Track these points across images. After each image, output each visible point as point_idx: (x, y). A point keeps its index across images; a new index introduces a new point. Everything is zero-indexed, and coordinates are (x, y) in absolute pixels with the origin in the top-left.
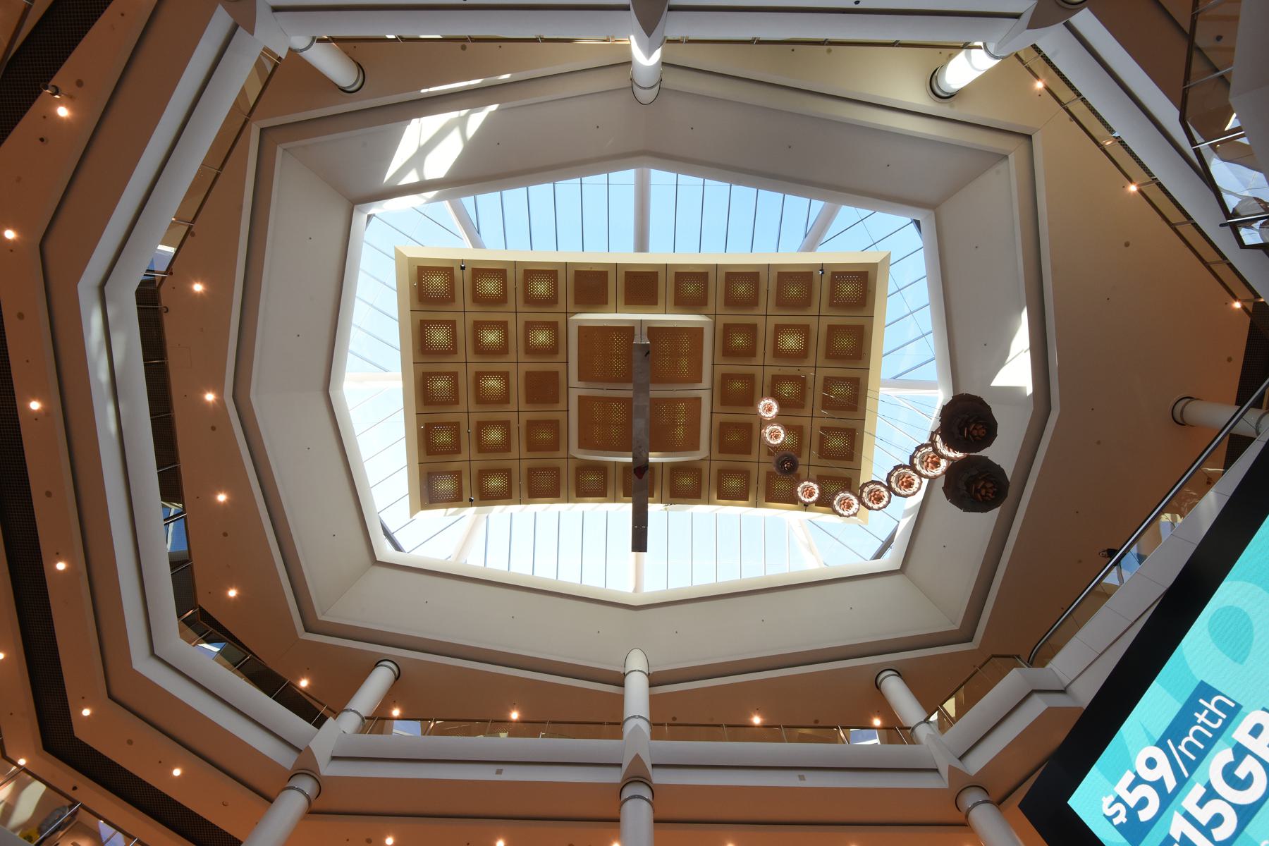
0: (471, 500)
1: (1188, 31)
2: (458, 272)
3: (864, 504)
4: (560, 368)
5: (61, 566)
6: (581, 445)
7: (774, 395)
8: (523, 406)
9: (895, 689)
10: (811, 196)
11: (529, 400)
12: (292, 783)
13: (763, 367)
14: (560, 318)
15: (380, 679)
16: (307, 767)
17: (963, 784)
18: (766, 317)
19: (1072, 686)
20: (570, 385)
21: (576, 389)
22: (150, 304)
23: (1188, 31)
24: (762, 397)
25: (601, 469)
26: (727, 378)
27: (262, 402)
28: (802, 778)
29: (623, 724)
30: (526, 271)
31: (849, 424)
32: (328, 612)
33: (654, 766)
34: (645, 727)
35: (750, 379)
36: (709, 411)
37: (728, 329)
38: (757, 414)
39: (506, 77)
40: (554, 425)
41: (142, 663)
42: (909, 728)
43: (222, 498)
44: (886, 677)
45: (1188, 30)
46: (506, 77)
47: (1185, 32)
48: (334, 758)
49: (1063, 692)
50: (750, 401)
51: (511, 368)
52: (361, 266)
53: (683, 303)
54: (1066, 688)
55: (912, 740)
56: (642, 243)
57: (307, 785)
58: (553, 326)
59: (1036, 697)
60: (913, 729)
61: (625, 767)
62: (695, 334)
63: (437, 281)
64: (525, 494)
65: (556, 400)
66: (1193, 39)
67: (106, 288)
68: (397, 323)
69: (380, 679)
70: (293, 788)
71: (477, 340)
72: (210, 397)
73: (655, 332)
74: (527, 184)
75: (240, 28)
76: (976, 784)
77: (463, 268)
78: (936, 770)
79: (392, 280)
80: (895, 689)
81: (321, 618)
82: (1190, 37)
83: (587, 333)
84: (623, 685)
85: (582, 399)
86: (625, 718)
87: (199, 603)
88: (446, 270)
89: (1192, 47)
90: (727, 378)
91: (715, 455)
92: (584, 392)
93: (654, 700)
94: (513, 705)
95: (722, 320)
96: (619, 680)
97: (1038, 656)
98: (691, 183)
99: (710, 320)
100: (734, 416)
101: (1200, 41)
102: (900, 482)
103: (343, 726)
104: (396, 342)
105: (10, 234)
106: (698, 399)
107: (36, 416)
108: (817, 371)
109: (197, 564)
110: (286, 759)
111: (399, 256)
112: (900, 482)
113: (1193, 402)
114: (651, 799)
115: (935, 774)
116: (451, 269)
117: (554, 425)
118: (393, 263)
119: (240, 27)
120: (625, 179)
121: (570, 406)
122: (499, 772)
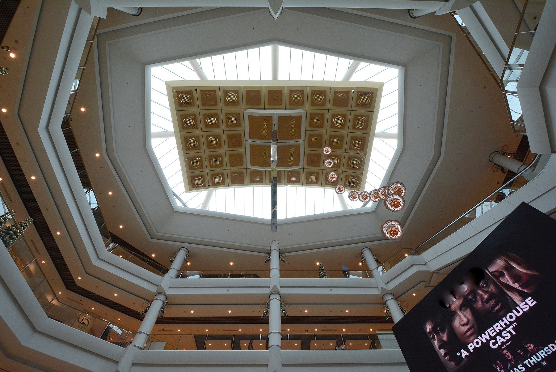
1: (521, 12)
3: (360, 199)
4: (242, 132)
6: (252, 164)
7: (330, 145)
9: (368, 255)
10: (350, 59)
11: (229, 147)
12: (155, 298)
13: (326, 132)
14: (241, 111)
16: (161, 292)
17: (386, 293)
18: (328, 110)
19: (428, 263)
20: (246, 140)
22: (67, 127)
23: (521, 12)
24: (326, 146)
25: (260, 173)
26: (311, 136)
28: (331, 290)
29: (270, 271)
33: (281, 287)
35: (320, 136)
36: (304, 130)
37: (312, 116)
40: (312, 125)
41: (96, 262)
42: (370, 271)
43: (110, 193)
44: (364, 251)
45: (521, 11)
47: (520, 12)
49: (425, 264)
50: (320, 146)
52: (152, 86)
53: (294, 104)
55: (372, 277)
58: (238, 115)
61: (271, 288)
62: (299, 118)
63: (185, 97)
64: (230, 182)
65: (240, 146)
66: (523, 15)
67: (49, 128)
71: (206, 122)
72: (97, 155)
73: (281, 119)
75: (82, 10)
76: (391, 293)
77: (196, 90)
78: (377, 287)
79: (165, 92)
80: (368, 255)
82: (522, 15)
83: (251, 118)
85: (251, 146)
87: (109, 230)
89: (522, 18)
90: (311, 136)
91: (306, 167)
92: (252, 143)
95: (309, 112)
96: (269, 252)
97: (418, 251)
98: (297, 52)
99: (305, 111)
100: (314, 151)
101: (525, 16)
102: (374, 196)
103: (172, 273)
105: (4, 110)
108: (349, 133)
109: (103, 213)
110: (154, 289)
112: (374, 196)
113: (499, 154)
115: (377, 289)
116: (192, 91)
119: (82, 9)
120: (267, 50)
122: (228, 291)
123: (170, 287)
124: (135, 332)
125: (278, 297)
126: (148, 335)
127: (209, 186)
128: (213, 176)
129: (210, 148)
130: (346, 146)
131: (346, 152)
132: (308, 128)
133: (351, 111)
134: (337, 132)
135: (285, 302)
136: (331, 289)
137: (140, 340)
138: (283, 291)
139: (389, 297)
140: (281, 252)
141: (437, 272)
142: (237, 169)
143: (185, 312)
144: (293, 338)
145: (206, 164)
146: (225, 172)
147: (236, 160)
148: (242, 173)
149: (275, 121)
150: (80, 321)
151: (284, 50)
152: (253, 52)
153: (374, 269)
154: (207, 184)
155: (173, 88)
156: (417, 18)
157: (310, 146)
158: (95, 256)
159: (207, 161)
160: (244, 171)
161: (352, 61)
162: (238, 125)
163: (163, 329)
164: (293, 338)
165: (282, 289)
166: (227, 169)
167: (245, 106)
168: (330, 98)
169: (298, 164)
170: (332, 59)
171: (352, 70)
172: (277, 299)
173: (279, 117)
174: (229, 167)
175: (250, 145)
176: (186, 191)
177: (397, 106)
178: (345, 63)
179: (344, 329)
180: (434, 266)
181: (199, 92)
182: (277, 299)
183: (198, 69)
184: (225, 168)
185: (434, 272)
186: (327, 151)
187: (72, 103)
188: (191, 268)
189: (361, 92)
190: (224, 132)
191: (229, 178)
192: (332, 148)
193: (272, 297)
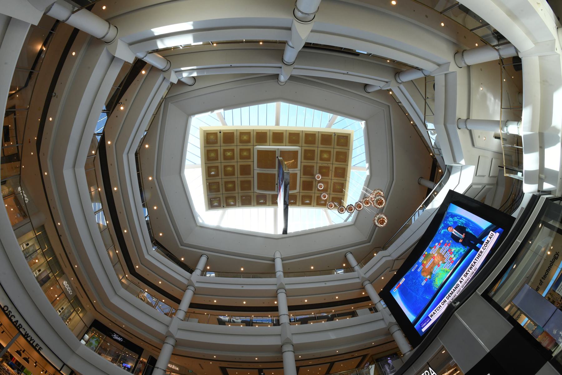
0: (223, 206)
2: (219, 134)
4: (251, 163)
5: (125, 231)
6: (258, 188)
8: (239, 176)
9: (351, 258)
12: (187, 288)
13: (317, 164)
14: (251, 147)
15: (203, 260)
16: (191, 284)
17: (364, 280)
18: (318, 148)
21: (256, 170)
25: (264, 197)
27: (164, 180)
28: (325, 284)
30: (240, 133)
31: (342, 182)
32: (186, 241)
34: (282, 274)
38: (315, 178)
39: (292, 201)
40: (249, 182)
41: (147, 257)
46: (292, 201)
48: (197, 282)
51: (235, 164)
54: (390, 255)
56: (277, 123)
57: (192, 288)
58: (249, 150)
59: (384, 258)
60: (354, 267)
62: (296, 153)
63: (212, 137)
68: (200, 149)
69: (203, 260)
70: (189, 289)
72: (150, 178)
74: (241, 107)
80: (351, 258)
81: (185, 242)
83: (260, 152)
84: (274, 261)
86: (276, 271)
88: (215, 134)
92: (259, 172)
93: (283, 265)
94: (242, 267)
95: (304, 148)
96: (273, 260)
97: (384, 248)
98: (294, 108)
103: (197, 272)
104: (199, 155)
106: (296, 174)
107: (116, 192)
108: (334, 165)
111: (201, 129)
114: (285, 292)
115: (358, 279)
117: (249, 182)
118: (199, 130)
120: (272, 106)
121: (254, 175)
122: (242, 287)
123: (197, 282)
124: (177, 310)
125: (284, 291)
126: (185, 312)
127: (223, 206)
128: (227, 198)
129: (234, 173)
130: (332, 173)
131: (332, 179)
132: (303, 161)
133: (335, 149)
134: (324, 164)
135: (289, 294)
136: (325, 283)
137: (181, 314)
138: (287, 287)
139: (367, 282)
140: (283, 260)
141: (397, 259)
142: (246, 192)
143: (210, 301)
144: (296, 321)
145: (222, 188)
146: (236, 195)
147: (246, 186)
148: (250, 196)
149: (278, 154)
150: (140, 296)
151: (284, 105)
152: (262, 107)
153: (377, 303)
154: (222, 205)
155: (204, 131)
156: (369, 93)
157: (304, 174)
158: (147, 253)
159: (223, 186)
160: (252, 194)
161: (331, 115)
162: (248, 157)
163: (194, 312)
164: (296, 321)
165: (286, 285)
166: (238, 192)
167: (255, 144)
168: (319, 139)
169: (295, 189)
170: (318, 113)
171: (331, 123)
172: (283, 292)
173: (281, 151)
174: (240, 191)
175: (258, 173)
176: (207, 210)
177: (363, 147)
178: (327, 116)
179: (333, 310)
180: (395, 256)
181: (222, 134)
182: (283, 292)
183: (223, 120)
184: (237, 191)
185: (395, 260)
186: (318, 177)
187: (141, 142)
188: (210, 271)
189: (340, 136)
190: (237, 163)
191: (240, 200)
192: (322, 176)
193: (279, 291)
